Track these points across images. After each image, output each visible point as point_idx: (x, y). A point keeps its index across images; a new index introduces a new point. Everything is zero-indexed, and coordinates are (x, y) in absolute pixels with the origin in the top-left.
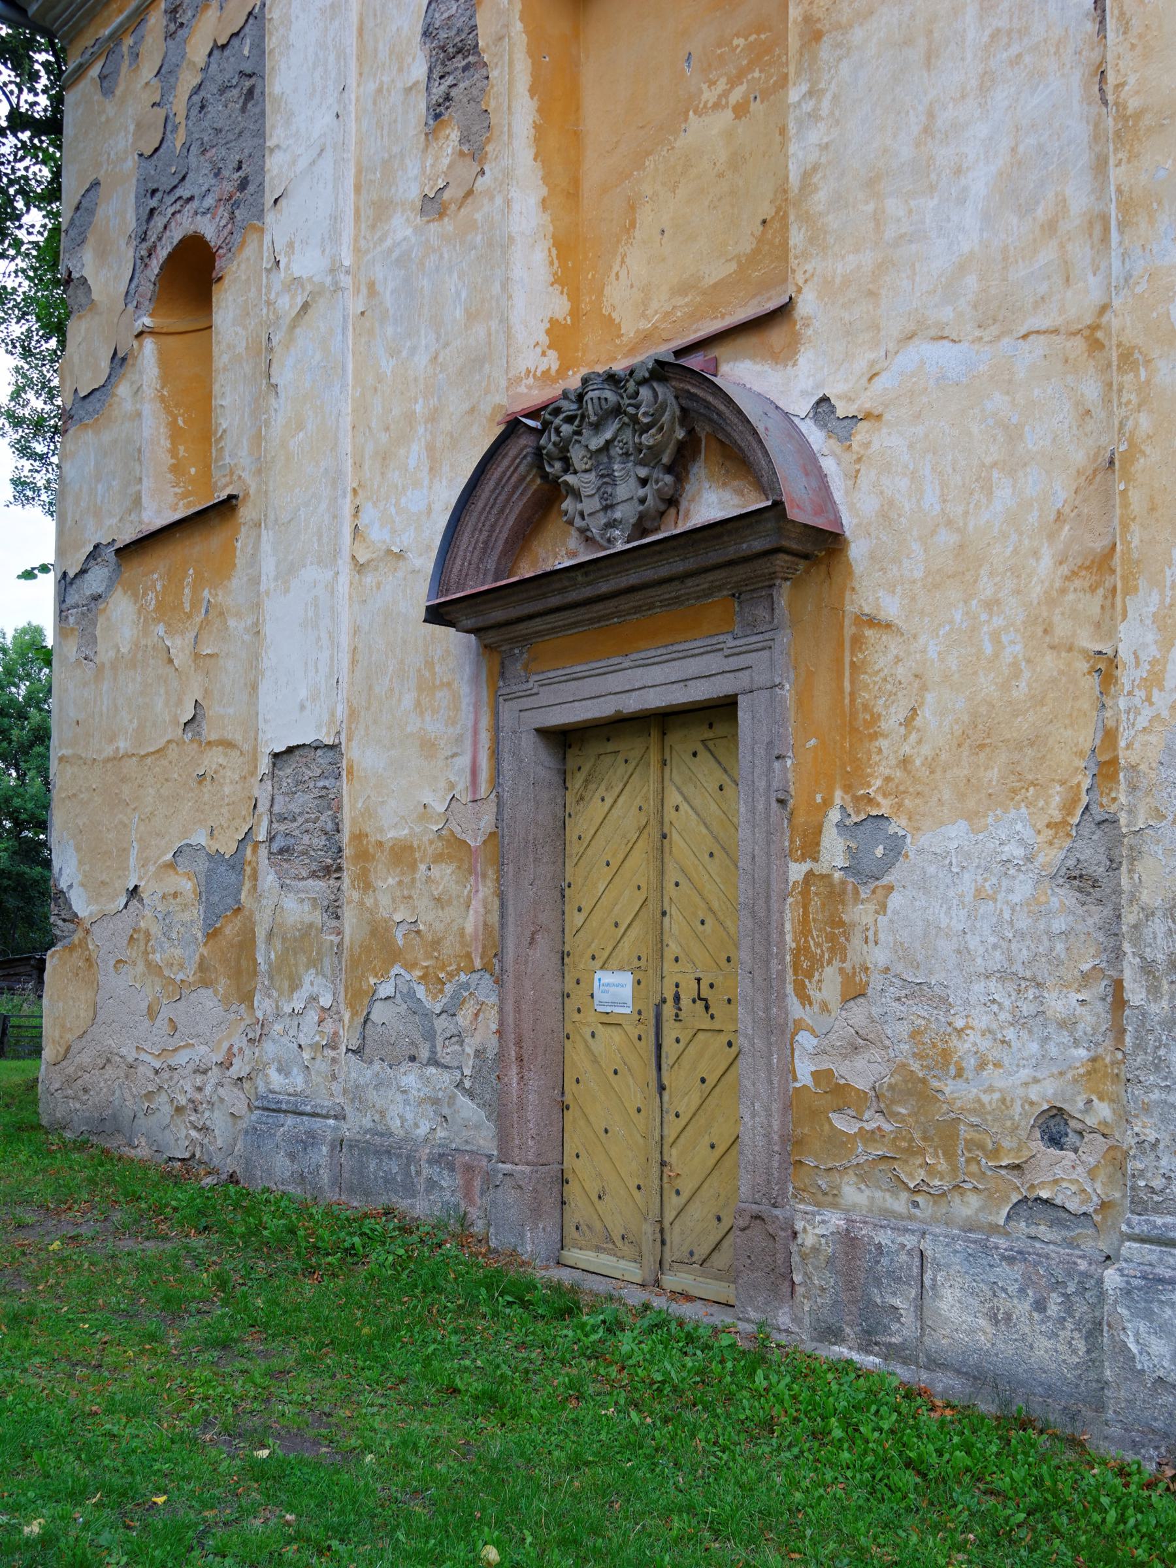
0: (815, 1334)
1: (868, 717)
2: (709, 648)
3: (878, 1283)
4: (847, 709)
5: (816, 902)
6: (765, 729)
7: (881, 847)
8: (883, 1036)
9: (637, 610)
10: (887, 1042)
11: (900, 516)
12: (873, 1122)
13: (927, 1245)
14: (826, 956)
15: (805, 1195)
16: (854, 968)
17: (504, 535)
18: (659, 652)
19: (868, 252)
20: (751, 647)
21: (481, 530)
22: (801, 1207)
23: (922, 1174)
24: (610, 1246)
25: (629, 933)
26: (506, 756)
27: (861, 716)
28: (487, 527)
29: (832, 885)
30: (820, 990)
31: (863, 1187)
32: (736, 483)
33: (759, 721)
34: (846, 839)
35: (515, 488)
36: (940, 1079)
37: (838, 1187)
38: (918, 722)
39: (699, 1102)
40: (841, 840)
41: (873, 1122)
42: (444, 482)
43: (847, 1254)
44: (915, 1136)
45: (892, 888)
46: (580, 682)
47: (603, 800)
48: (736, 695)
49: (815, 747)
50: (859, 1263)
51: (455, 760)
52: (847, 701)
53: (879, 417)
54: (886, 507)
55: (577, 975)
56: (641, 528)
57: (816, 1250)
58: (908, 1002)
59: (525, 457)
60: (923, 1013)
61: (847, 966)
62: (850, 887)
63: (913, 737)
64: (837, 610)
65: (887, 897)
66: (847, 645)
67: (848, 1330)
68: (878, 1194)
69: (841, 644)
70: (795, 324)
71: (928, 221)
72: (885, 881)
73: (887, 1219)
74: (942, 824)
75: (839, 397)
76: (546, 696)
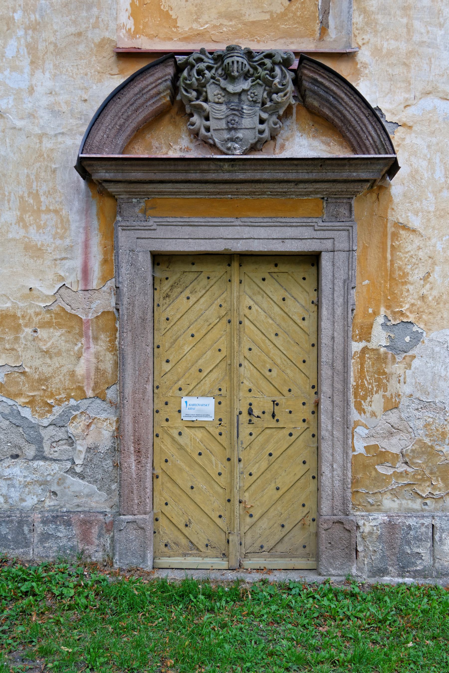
0: (370, 574)
1: (401, 273)
2: (304, 224)
3: (408, 543)
4: (389, 269)
5: (368, 363)
6: (342, 272)
7: (408, 337)
8: (408, 427)
9: (251, 193)
10: (410, 430)
11: (421, 179)
12: (401, 468)
13: (437, 523)
14: (375, 389)
15: (360, 507)
16: (391, 395)
17: (133, 125)
18: (265, 220)
19: (403, 43)
20: (335, 228)
21: (119, 118)
22: (358, 513)
23: (430, 490)
24: (195, 552)
25: (209, 375)
26: (124, 265)
27: (397, 273)
28: (124, 117)
29: (379, 354)
30: (371, 406)
31: (396, 499)
32: (324, 138)
33: (338, 268)
34: (387, 332)
35: (152, 97)
36: (440, 446)
37: (381, 501)
38: (431, 279)
39: (267, 466)
40: (384, 333)
41: (401, 468)
42: (47, 75)
43: (389, 532)
44: (426, 473)
45: (415, 357)
46: (195, 228)
47: (188, 298)
48: (321, 252)
49: (368, 285)
50: (397, 535)
51: (64, 262)
52: (389, 264)
53: (410, 127)
54: (414, 173)
55: (166, 400)
56: (253, 148)
57: (371, 533)
58: (422, 411)
59: (166, 81)
60: (432, 416)
61: (388, 394)
62: (390, 356)
63: (428, 286)
64: (383, 218)
65: (411, 361)
66: (389, 236)
67: (390, 568)
68: (404, 502)
69: (385, 235)
70: (357, 64)
71: (438, 40)
72: (411, 353)
73: (410, 514)
74: (443, 328)
75: (387, 111)
76: (161, 232)
